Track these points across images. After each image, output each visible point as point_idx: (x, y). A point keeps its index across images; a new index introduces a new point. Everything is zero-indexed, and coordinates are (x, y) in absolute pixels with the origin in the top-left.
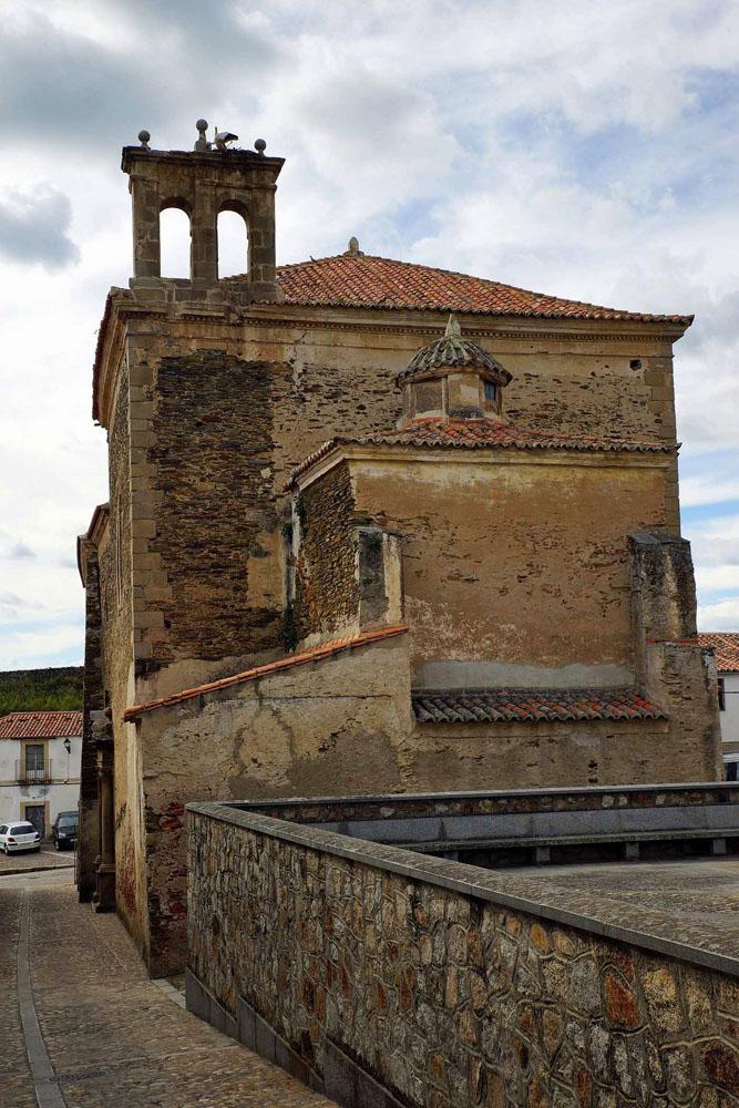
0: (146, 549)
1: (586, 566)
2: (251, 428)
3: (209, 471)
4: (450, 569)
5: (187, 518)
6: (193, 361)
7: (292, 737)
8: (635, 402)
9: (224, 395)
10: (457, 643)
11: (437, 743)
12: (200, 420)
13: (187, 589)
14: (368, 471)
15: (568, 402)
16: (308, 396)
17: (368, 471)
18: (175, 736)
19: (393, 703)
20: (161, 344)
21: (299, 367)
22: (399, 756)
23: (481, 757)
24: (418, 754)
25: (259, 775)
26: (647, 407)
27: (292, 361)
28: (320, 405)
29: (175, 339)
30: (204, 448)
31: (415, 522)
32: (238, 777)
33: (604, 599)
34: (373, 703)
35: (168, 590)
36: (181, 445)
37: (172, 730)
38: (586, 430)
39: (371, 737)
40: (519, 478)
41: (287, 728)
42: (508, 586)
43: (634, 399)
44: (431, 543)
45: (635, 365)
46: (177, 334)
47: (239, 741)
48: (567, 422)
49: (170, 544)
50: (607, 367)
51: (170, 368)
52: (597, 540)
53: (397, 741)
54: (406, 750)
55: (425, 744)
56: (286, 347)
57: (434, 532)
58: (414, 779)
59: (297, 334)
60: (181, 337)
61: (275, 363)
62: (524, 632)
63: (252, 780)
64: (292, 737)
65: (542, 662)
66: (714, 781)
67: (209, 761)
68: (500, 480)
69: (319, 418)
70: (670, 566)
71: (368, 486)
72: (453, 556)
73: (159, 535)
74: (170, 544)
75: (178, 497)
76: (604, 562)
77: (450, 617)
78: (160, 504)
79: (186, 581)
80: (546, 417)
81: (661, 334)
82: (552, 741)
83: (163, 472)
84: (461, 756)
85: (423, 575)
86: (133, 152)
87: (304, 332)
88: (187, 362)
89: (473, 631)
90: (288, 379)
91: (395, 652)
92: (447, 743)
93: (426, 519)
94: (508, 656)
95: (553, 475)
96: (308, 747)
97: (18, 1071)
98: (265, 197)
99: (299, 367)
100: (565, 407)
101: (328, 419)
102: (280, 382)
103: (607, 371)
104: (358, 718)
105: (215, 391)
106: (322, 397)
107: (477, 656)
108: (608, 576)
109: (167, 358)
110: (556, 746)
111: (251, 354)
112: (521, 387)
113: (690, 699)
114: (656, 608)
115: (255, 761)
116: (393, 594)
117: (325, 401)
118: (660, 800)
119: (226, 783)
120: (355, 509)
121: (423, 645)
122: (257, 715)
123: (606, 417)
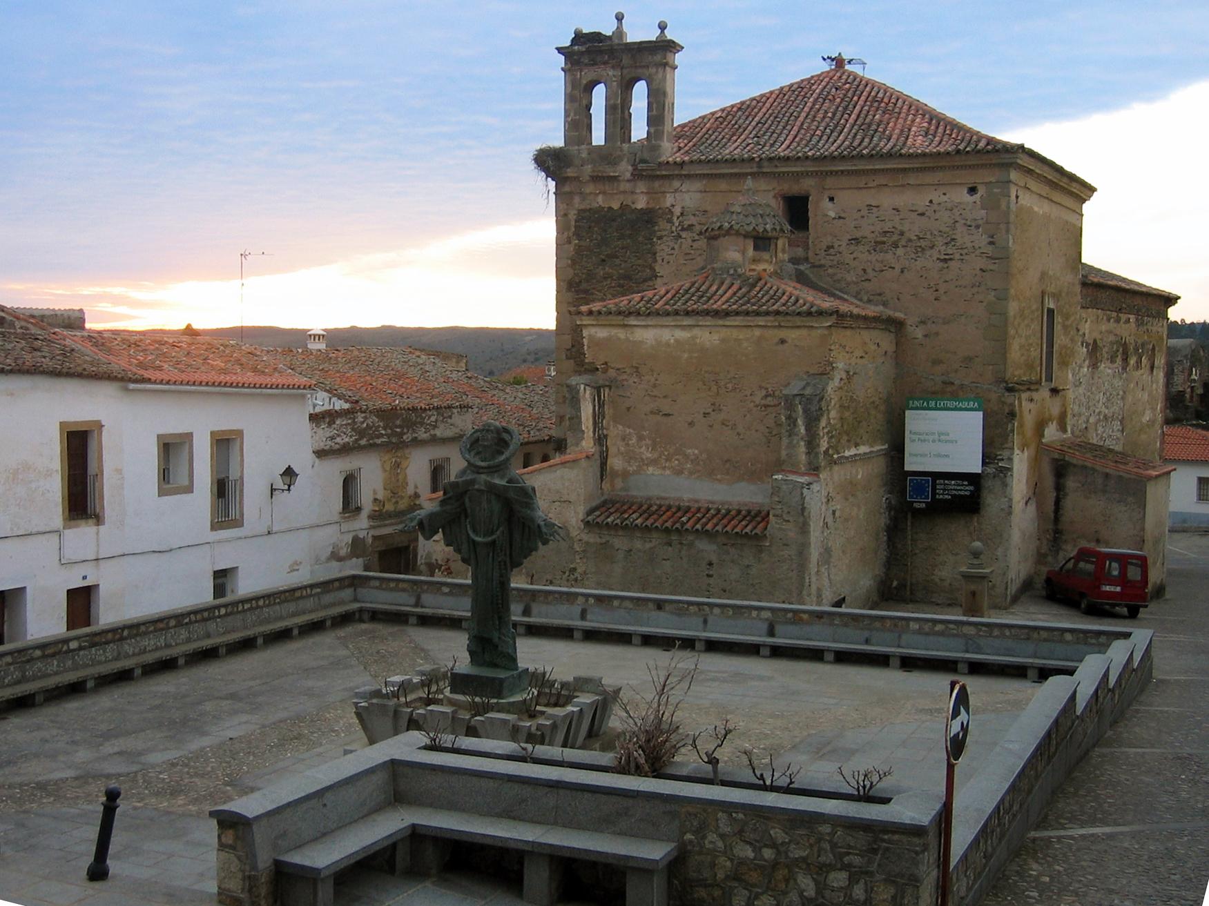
0: (564, 357)
1: (757, 406)
2: (640, 262)
8: (970, 226)
9: (622, 237)
10: (654, 462)
11: (600, 537)
12: (603, 257)
15: (905, 229)
16: (684, 234)
21: (677, 211)
23: (631, 550)
24: (587, 543)
27: (673, 206)
28: (694, 241)
30: (605, 278)
31: (628, 370)
33: (771, 433)
38: (920, 254)
40: (708, 336)
43: (969, 223)
45: (972, 190)
48: (904, 246)
50: (944, 194)
51: (583, 218)
52: (768, 386)
53: (574, 533)
54: (580, 540)
55: (588, 537)
56: (668, 195)
58: (585, 560)
59: (676, 184)
60: (591, 193)
61: (660, 208)
62: (705, 456)
65: (717, 480)
68: (694, 338)
69: (692, 252)
71: (597, 344)
72: (655, 396)
73: (573, 346)
76: (772, 403)
80: (884, 243)
82: (681, 543)
83: (577, 299)
86: (643, 45)
89: (666, 453)
90: (670, 221)
91: (575, 471)
92: (608, 538)
93: (637, 368)
94: (691, 473)
95: (735, 333)
97: (1048, 764)
98: (657, 72)
99: (677, 211)
100: (902, 234)
101: (699, 252)
102: (662, 224)
103: (945, 198)
106: (694, 235)
108: (774, 415)
109: (582, 210)
110: (685, 548)
111: (641, 203)
112: (863, 217)
113: (788, 521)
114: (791, 446)
116: (587, 428)
117: (697, 238)
118: (616, 603)
121: (629, 462)
123: (940, 241)
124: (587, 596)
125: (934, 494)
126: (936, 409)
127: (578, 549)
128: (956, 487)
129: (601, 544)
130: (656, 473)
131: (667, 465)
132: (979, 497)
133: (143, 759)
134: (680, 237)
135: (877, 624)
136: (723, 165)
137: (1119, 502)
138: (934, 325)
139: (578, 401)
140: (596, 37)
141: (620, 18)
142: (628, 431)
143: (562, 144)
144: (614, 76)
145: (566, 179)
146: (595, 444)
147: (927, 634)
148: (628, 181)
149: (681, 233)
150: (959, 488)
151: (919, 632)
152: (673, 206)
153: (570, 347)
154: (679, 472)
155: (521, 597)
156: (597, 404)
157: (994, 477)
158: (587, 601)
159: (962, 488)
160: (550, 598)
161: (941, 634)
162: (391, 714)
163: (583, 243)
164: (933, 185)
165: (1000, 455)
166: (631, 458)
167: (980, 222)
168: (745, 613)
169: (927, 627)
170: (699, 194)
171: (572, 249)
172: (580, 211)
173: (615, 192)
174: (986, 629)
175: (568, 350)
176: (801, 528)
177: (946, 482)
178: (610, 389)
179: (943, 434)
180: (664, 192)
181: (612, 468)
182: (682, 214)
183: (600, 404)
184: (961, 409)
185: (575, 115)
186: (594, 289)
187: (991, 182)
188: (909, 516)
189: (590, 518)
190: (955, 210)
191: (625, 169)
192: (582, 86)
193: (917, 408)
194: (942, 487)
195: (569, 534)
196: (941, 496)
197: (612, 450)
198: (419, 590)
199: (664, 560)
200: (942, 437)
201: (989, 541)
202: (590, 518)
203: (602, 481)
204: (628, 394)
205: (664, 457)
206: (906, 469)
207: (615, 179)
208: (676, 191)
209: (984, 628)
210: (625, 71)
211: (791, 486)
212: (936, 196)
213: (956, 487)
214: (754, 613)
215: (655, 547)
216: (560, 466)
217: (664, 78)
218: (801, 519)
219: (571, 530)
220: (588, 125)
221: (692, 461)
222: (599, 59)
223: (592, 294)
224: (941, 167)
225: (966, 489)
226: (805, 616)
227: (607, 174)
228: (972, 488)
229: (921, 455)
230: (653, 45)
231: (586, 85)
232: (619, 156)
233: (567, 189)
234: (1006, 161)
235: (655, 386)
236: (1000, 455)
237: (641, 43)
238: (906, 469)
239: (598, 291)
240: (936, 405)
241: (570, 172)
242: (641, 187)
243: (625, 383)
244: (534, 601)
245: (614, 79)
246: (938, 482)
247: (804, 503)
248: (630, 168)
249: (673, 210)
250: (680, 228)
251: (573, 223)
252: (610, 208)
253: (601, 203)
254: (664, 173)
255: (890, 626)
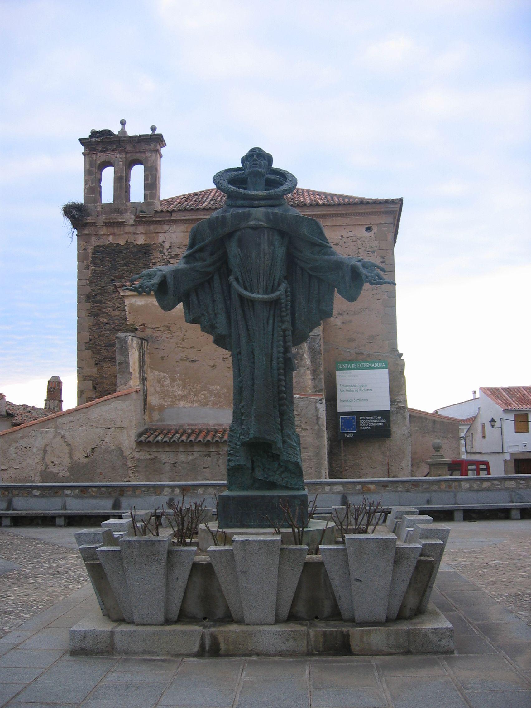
0: (84, 348)
3: (118, 305)
4: (182, 355)
5: (105, 331)
6: (109, 246)
7: (71, 450)
8: (368, 251)
10: (183, 397)
11: (150, 454)
13: (105, 368)
14: (136, 301)
16: (172, 261)
17: (136, 301)
18: (16, 448)
19: (125, 432)
20: (93, 239)
21: (167, 245)
22: (128, 461)
23: (176, 463)
24: (139, 460)
25: (55, 470)
26: (375, 254)
29: (101, 235)
32: (44, 471)
34: (115, 432)
35: (95, 370)
36: (103, 290)
37: (14, 445)
39: (113, 450)
41: (69, 445)
42: (216, 364)
43: (368, 249)
44: (172, 340)
45: (368, 229)
46: (102, 233)
47: (45, 451)
49: (96, 345)
50: (351, 231)
53: (127, 453)
55: (143, 455)
56: (160, 235)
57: (173, 334)
58: (136, 474)
59: (166, 227)
60: (104, 234)
63: (51, 472)
64: (71, 450)
66: (320, 478)
67: (30, 461)
70: (306, 349)
71: (135, 309)
72: (183, 348)
73: (90, 340)
74: (96, 345)
75: (101, 320)
77: (180, 383)
78: (91, 324)
79: (104, 364)
81: (383, 210)
82: (219, 454)
83: (93, 307)
84: (164, 462)
85: (165, 358)
86: (142, 138)
87: (170, 226)
88: (107, 248)
89: (194, 390)
90: (161, 252)
91: (127, 403)
92: (156, 454)
93: (168, 326)
94: (215, 404)
96: (80, 456)
99: (167, 245)
102: (156, 254)
103: (351, 234)
104: (106, 440)
105: (122, 262)
107: (196, 404)
110: (221, 457)
111: (141, 240)
113: (306, 429)
115: (52, 462)
116: (134, 370)
118: (200, 491)
119: (39, 474)
120: (128, 323)
121: (164, 399)
122: (54, 437)
124: (172, 487)
125: (359, 427)
126: (357, 369)
127: (131, 466)
128: (373, 421)
129: (150, 459)
130: (186, 406)
131: (195, 399)
132: (389, 426)
133: (529, 599)
134: (169, 263)
135: (435, 487)
136: (201, 213)
137: (443, 437)
138: (347, 316)
139: (127, 350)
140: (107, 133)
141: (123, 123)
142: (162, 374)
143: (83, 202)
144: (120, 158)
145: (85, 225)
146: (140, 383)
147: (477, 491)
148: (132, 225)
149: (170, 260)
150: (376, 421)
151: (470, 490)
152: (163, 242)
153: (88, 340)
154: (205, 404)
155: (110, 493)
156: (141, 352)
157: (397, 413)
158: (173, 491)
159: (378, 421)
160: (138, 492)
161: (488, 490)
162: (164, 558)
163: (97, 269)
164: (343, 225)
165: (398, 399)
166: (165, 396)
167: (375, 249)
168: (319, 488)
169: (475, 486)
170: (182, 233)
171: (90, 273)
172: (96, 247)
173: (122, 233)
174: (524, 482)
175: (86, 343)
176: (316, 434)
177: (367, 418)
178: (148, 343)
179: (362, 386)
180: (158, 233)
181: (150, 404)
182: (170, 247)
183: (142, 353)
184: (373, 368)
185: (92, 184)
186: (106, 300)
187: (381, 224)
188: (342, 443)
189: (142, 438)
190: (358, 242)
191: (129, 218)
192: (97, 165)
193: (344, 369)
194: (364, 421)
195: (123, 453)
196: (364, 428)
197: (151, 390)
198: (10, 495)
199: (204, 468)
200: (363, 388)
201: (396, 457)
202: (142, 438)
203: (144, 413)
204: (163, 347)
205: (192, 393)
206: (340, 410)
207: (122, 224)
208: (166, 232)
209: (522, 482)
210: (128, 155)
211: (308, 402)
212: (346, 233)
213: (373, 421)
214: (327, 488)
215: (196, 459)
216: (114, 399)
217: (156, 160)
218: (317, 427)
219: (124, 449)
220: (99, 191)
221: (215, 395)
222: (109, 147)
223: (105, 303)
224: (349, 214)
225: (380, 422)
226: (372, 487)
227: (116, 221)
228: (384, 421)
229: (348, 401)
230: (149, 137)
231: (100, 164)
232: (125, 209)
233: (86, 232)
234: (391, 209)
235: (183, 340)
236: (398, 399)
237: (140, 136)
238: (340, 410)
239: (109, 301)
240: (357, 366)
241: (89, 220)
242: (141, 229)
243: (159, 338)
244: (122, 496)
245: (120, 160)
246: (361, 418)
247: (318, 414)
248: (133, 217)
249: (164, 245)
250: (169, 257)
251: (90, 255)
252: (118, 244)
253: (111, 241)
254: (158, 219)
255: (446, 487)
